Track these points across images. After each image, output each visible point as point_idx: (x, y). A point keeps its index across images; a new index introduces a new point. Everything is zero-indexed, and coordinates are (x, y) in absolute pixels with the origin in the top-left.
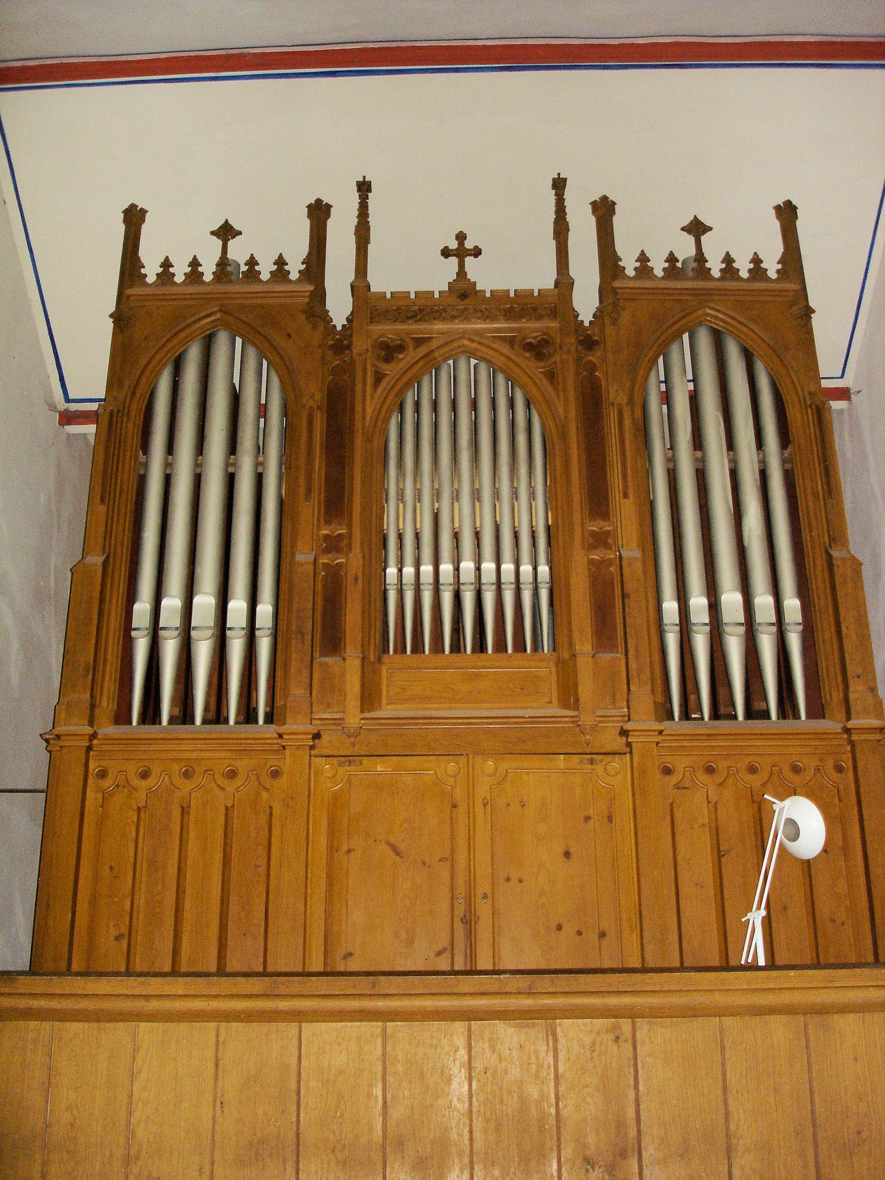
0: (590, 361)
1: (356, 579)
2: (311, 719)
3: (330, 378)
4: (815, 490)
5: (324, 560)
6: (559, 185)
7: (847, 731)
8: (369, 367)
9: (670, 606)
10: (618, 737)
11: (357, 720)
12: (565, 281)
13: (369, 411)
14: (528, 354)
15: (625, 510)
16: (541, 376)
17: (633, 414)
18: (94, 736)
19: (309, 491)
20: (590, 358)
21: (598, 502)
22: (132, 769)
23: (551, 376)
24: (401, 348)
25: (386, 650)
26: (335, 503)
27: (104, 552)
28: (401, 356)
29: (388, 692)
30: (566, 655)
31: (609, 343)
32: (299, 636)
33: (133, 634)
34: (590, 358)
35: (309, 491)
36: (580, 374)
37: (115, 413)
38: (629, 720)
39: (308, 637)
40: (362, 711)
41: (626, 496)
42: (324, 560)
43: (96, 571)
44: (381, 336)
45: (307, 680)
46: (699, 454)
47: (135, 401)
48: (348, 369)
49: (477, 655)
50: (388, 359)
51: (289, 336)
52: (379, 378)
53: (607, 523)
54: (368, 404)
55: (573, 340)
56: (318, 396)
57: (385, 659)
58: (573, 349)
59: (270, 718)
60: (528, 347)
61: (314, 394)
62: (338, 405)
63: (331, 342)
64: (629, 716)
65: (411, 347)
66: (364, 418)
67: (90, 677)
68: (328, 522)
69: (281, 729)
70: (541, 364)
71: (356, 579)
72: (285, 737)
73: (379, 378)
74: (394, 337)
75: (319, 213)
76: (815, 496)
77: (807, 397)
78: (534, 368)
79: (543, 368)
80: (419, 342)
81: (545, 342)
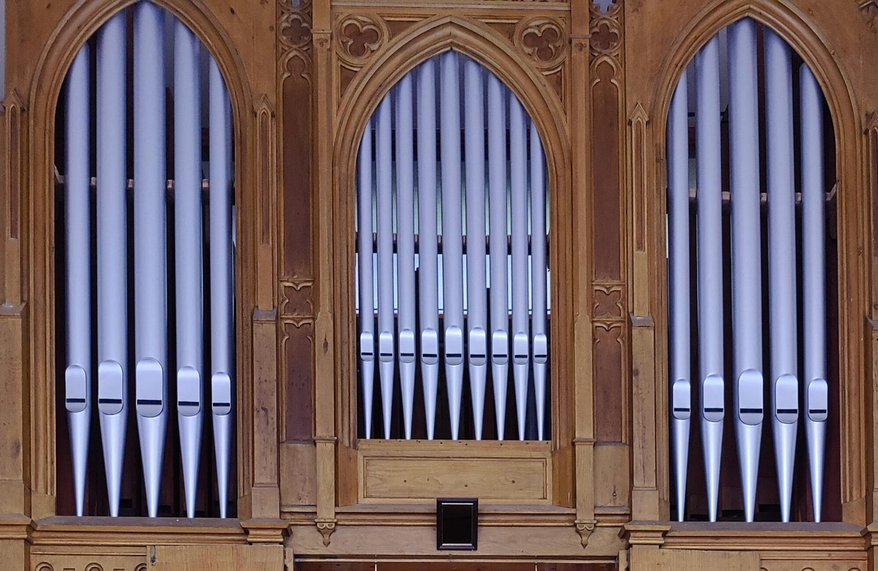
0: (605, 62)
1: (326, 345)
2: (281, 512)
3: (286, 76)
4: (860, 245)
5: (289, 318)
7: (867, 535)
8: (334, 54)
9: (682, 390)
10: (618, 539)
11: (332, 516)
12: (366, 465)
13: (336, 121)
14: (528, 50)
15: (640, 263)
16: (544, 81)
17: (654, 136)
18: (31, 528)
19: (265, 232)
20: (606, 58)
21: (608, 253)
23: (558, 82)
24: (374, 36)
25: (361, 434)
26: (300, 245)
27: (22, 301)
28: (375, 47)
29: (365, 484)
30: (564, 444)
31: (630, 38)
32: (262, 412)
33: (68, 405)
34: (606, 58)
35: (265, 232)
36: (594, 80)
37: (19, 111)
38: (630, 520)
39: (273, 415)
40: (336, 505)
41: (640, 247)
42: (289, 318)
43: (14, 324)
44: (349, 17)
45: (274, 467)
46: (726, 196)
47: (43, 97)
48: (309, 63)
49: (464, 442)
50: (358, 51)
51: (233, 11)
52: (347, 77)
53: (616, 282)
54: (332, 118)
55: (587, 32)
56: (272, 99)
57: (361, 444)
58: (587, 42)
59: (232, 511)
60: (531, 39)
61: (265, 88)
62: (298, 109)
63: (284, 25)
64: (630, 515)
65: (386, 37)
66: (330, 132)
67: (21, 457)
68: (291, 272)
69: (245, 525)
70: (546, 65)
71: (326, 345)
72: (251, 532)
73: (347, 77)
74: (366, 19)
76: (859, 251)
77: (863, 120)
78: (534, 70)
79: (548, 70)
81: (551, 35)
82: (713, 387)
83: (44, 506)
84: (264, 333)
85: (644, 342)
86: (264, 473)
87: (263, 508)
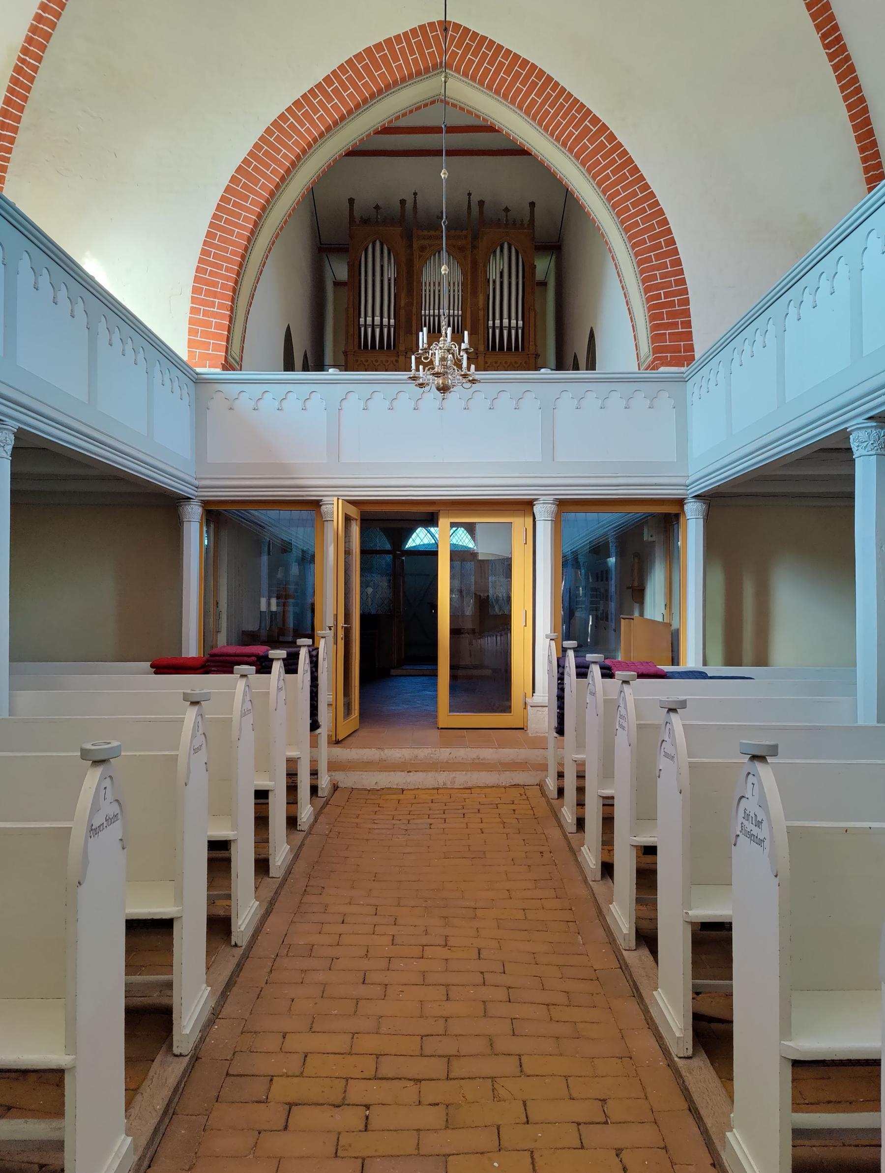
6: (470, 194)
9: (491, 323)
15: (481, 298)
21: (475, 294)
22: (363, 360)
24: (426, 248)
52: (420, 256)
62: (410, 263)
73: (420, 256)
75: (403, 202)
80: (430, 246)
82: (498, 322)
83: (356, 348)
84: (402, 312)
85: (481, 313)
86: (402, 339)
87: (402, 347)
